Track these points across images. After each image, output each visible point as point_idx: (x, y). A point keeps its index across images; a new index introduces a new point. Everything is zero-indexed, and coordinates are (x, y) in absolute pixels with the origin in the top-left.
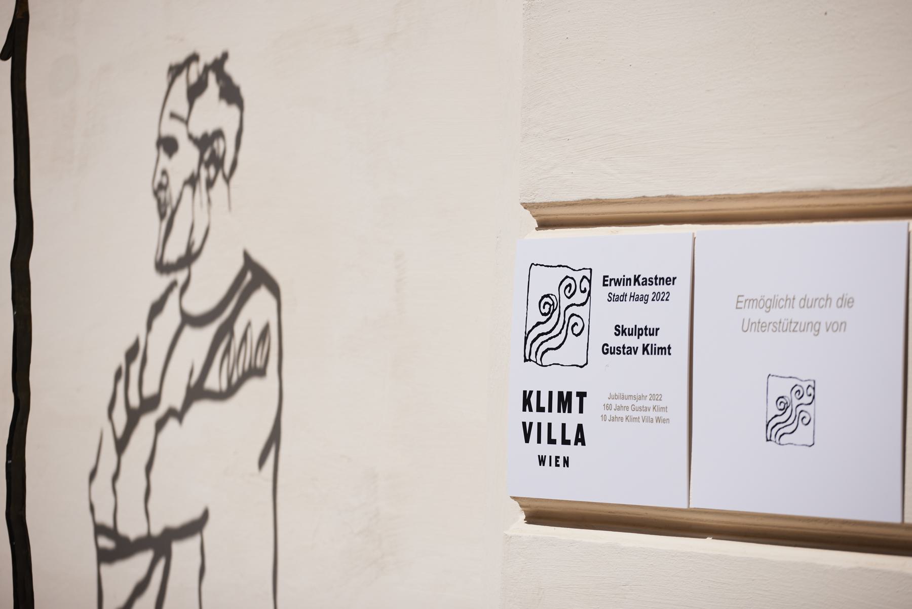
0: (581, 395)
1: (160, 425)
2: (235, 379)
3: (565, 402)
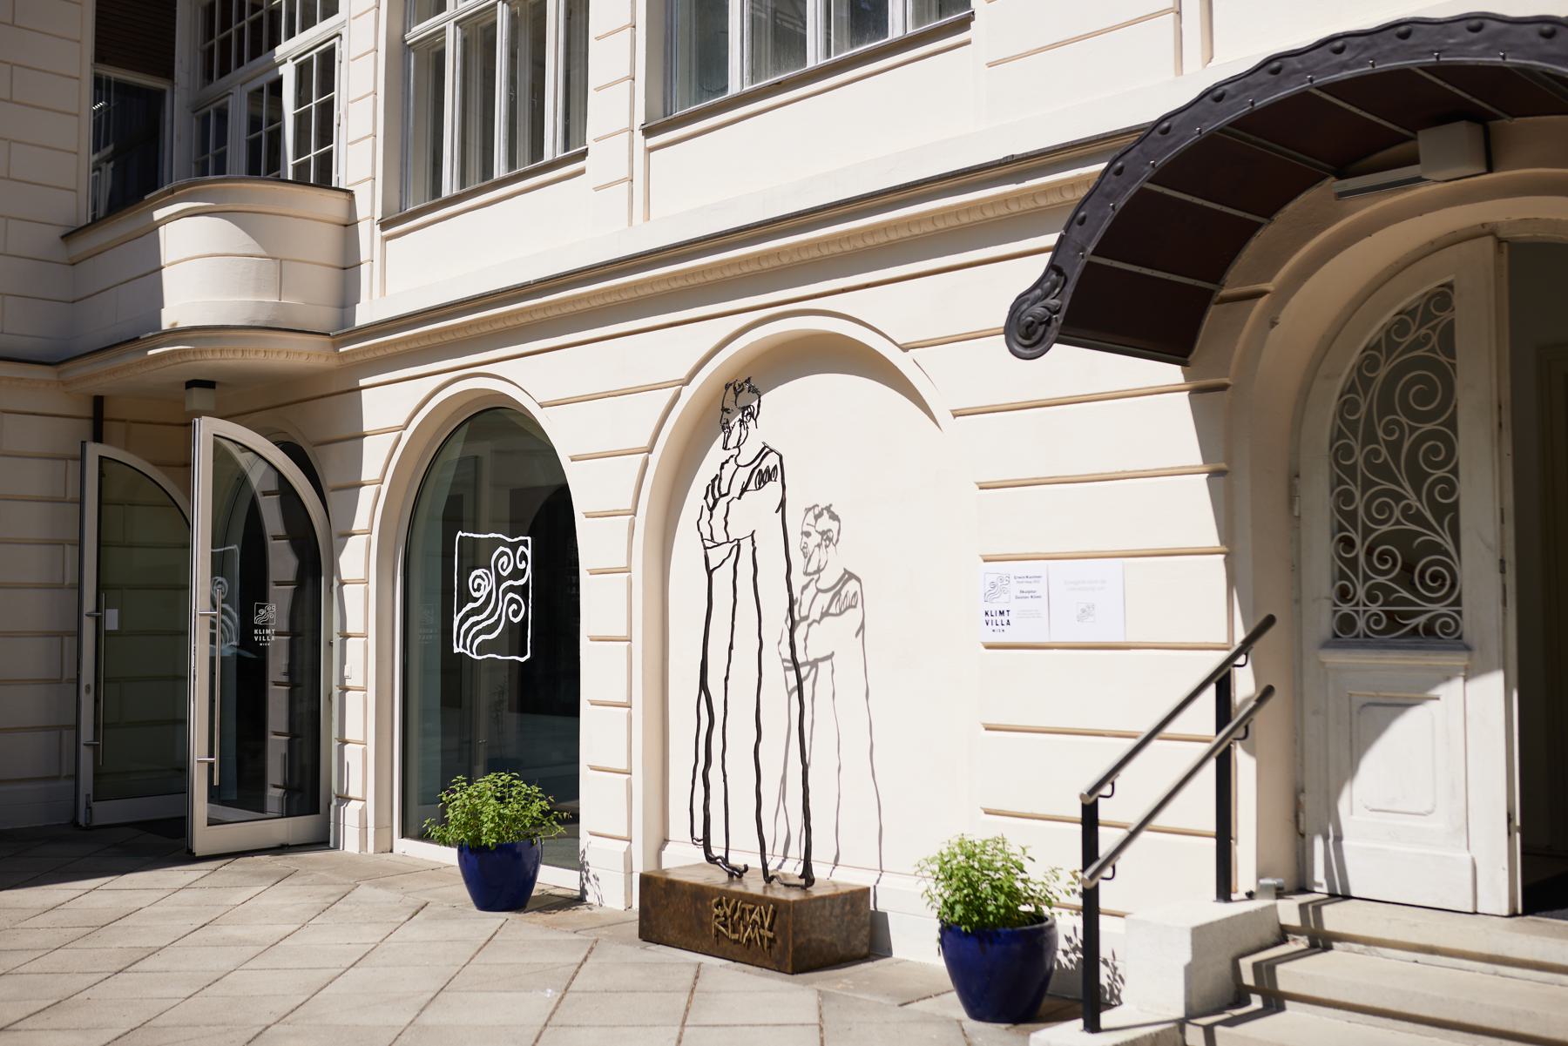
3: (1002, 613)
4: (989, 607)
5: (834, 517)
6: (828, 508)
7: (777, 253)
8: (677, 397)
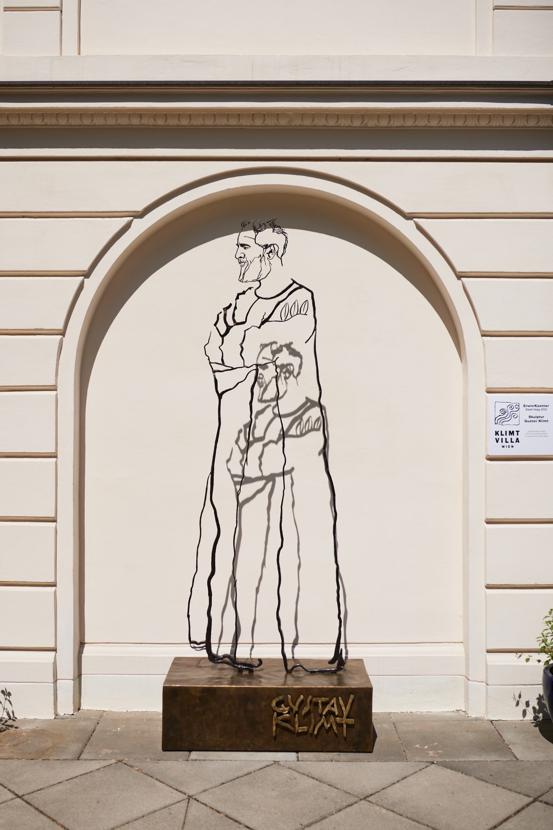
0: (518, 432)
1: (265, 445)
2: (304, 431)
3: (512, 433)
4: (499, 428)
5: (294, 353)
6: (288, 346)
7: (404, 114)
8: (127, 227)
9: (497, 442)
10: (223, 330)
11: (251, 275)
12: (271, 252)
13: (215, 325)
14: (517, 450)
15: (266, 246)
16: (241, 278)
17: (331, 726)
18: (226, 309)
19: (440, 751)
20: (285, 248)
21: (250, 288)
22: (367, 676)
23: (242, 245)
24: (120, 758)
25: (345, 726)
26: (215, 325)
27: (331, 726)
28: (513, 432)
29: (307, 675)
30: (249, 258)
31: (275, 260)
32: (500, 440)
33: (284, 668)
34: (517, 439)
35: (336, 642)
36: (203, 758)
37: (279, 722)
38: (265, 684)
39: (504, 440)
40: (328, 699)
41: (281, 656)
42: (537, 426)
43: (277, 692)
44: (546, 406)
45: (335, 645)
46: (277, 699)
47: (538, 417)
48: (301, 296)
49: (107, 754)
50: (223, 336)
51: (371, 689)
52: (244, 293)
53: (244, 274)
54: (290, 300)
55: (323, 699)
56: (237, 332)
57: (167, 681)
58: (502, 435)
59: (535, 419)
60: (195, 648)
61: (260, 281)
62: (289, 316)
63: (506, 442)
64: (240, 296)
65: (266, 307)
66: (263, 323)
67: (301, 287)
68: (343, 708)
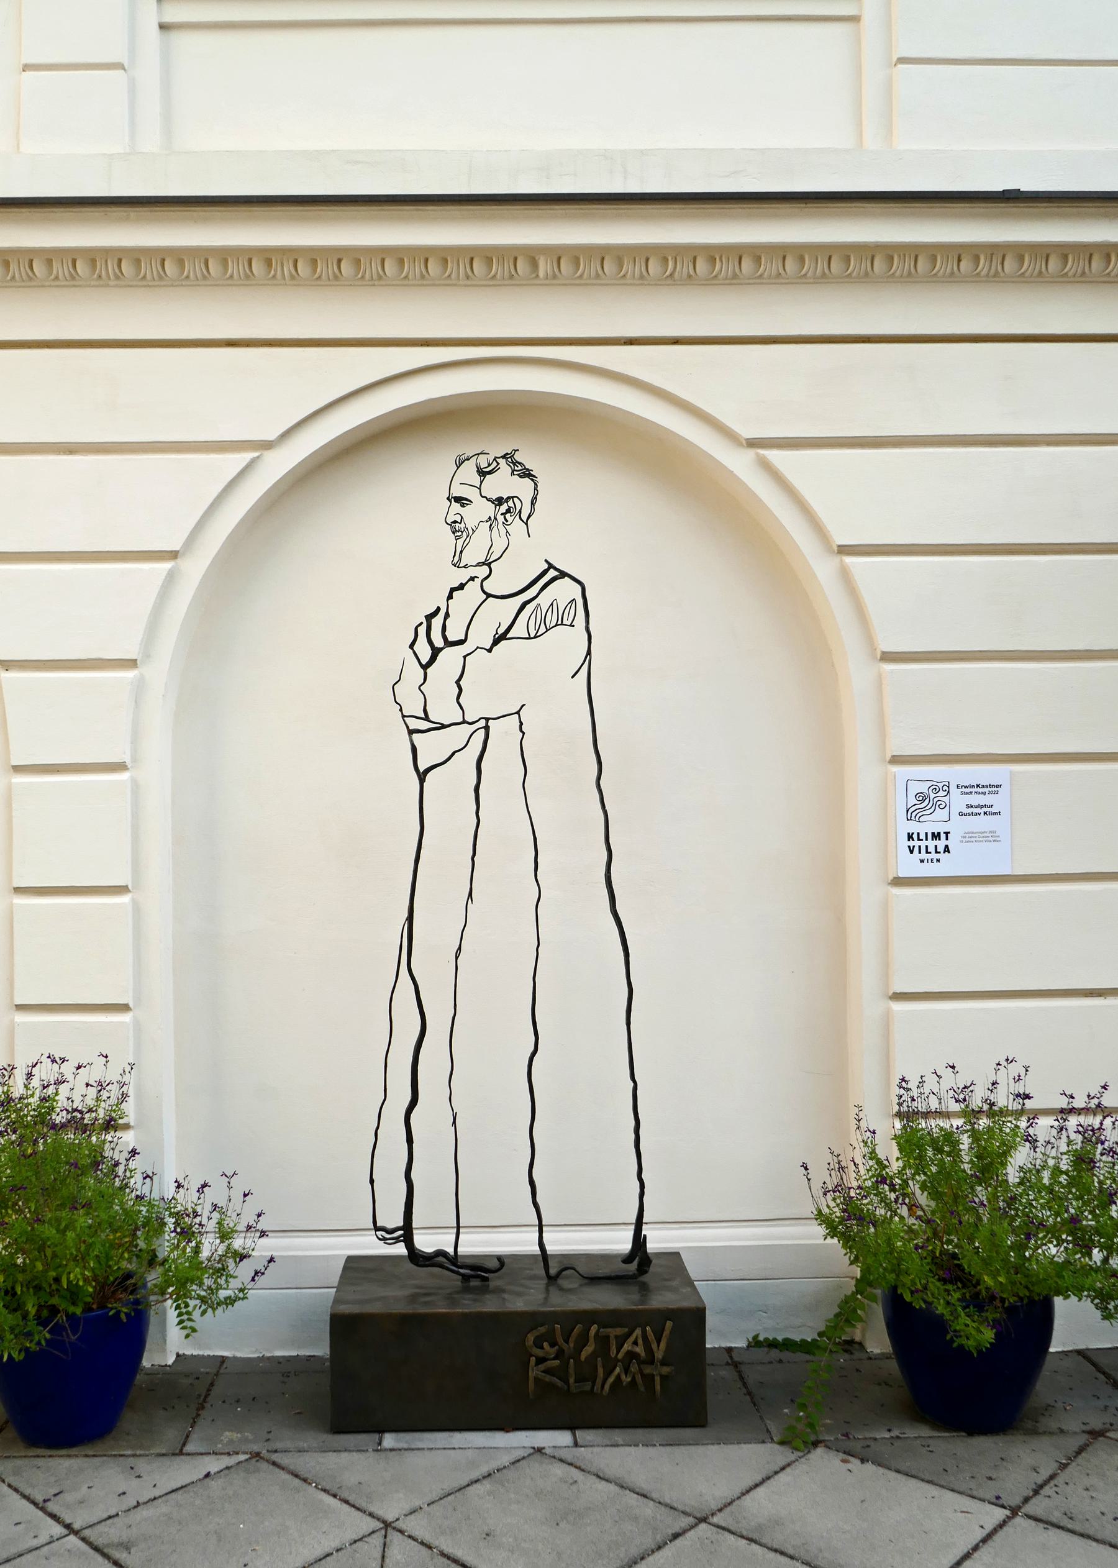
0: (947, 833)
3: (936, 836)
4: (914, 827)
9: (912, 852)
10: (425, 654)
11: (474, 553)
12: (508, 511)
13: (412, 646)
14: (946, 867)
15: (500, 501)
16: (456, 560)
17: (634, 1378)
18: (429, 617)
19: (828, 1421)
20: (533, 504)
21: (472, 579)
22: (690, 1283)
23: (458, 500)
24: (255, 1448)
25: (657, 1379)
26: (412, 646)
27: (634, 1378)
28: (939, 833)
29: (586, 1284)
30: (470, 523)
31: (517, 526)
32: (916, 850)
33: (543, 1272)
34: (947, 846)
35: (634, 1221)
36: (405, 1446)
37: (541, 1375)
38: (519, 1305)
39: (923, 850)
40: (626, 1330)
41: (536, 1249)
42: (982, 823)
43: (533, 1319)
44: (997, 786)
45: (633, 1227)
46: (535, 1333)
47: (982, 807)
48: (564, 591)
49: (231, 1441)
50: (425, 667)
51: (705, 1309)
52: (461, 587)
53: (461, 552)
54: (544, 600)
55: (619, 1331)
56: (450, 658)
57: (337, 1301)
58: (919, 839)
59: (978, 810)
60: (384, 1239)
61: (489, 565)
62: (543, 629)
63: (927, 852)
64: (455, 594)
65: (501, 613)
66: (496, 642)
67: (563, 574)
68: (654, 1346)
